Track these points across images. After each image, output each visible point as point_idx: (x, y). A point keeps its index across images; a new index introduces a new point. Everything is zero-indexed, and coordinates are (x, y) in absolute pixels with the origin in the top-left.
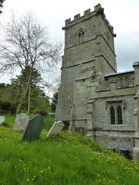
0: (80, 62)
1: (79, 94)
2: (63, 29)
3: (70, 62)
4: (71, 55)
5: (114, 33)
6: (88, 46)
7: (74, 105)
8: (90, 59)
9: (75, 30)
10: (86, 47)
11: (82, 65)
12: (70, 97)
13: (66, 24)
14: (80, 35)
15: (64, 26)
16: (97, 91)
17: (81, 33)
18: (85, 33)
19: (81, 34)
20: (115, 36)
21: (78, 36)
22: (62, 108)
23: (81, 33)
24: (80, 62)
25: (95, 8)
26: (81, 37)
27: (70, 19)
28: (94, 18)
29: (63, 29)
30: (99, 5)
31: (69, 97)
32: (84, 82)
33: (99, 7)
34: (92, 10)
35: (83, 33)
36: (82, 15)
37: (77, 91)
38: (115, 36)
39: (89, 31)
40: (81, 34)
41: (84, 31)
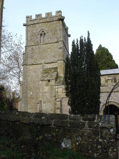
0: (43, 61)
1: (45, 92)
2: (24, 25)
3: (32, 60)
4: (33, 53)
5: (69, 33)
6: (50, 48)
7: (41, 101)
8: (52, 60)
9: (38, 29)
10: (48, 48)
11: (45, 64)
12: (33, 93)
13: (27, 21)
14: (41, 35)
15: (25, 23)
16: (63, 92)
17: (43, 33)
18: (47, 34)
19: (43, 35)
20: (69, 36)
21: (39, 36)
22: (25, 104)
23: (43, 33)
24: (43, 61)
25: (56, 13)
26: (42, 39)
27: (31, 16)
28: (55, 22)
29: (24, 25)
30: (60, 12)
31: (31, 93)
32: (49, 82)
33: (60, 14)
34: (54, 14)
35: (45, 34)
36: (44, 16)
37: (43, 89)
38: (69, 36)
39: (50, 34)
40: (43, 35)
41: (46, 33)
